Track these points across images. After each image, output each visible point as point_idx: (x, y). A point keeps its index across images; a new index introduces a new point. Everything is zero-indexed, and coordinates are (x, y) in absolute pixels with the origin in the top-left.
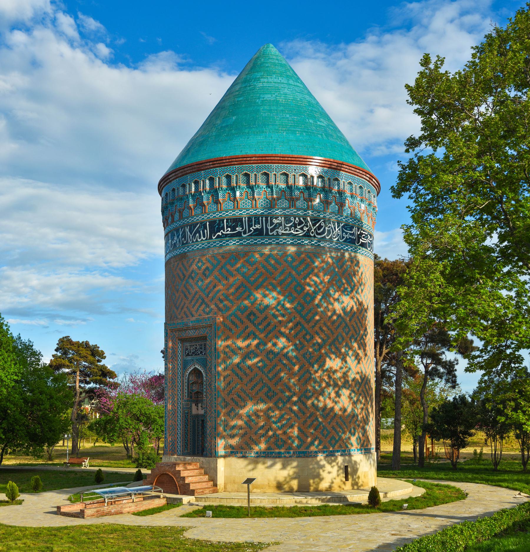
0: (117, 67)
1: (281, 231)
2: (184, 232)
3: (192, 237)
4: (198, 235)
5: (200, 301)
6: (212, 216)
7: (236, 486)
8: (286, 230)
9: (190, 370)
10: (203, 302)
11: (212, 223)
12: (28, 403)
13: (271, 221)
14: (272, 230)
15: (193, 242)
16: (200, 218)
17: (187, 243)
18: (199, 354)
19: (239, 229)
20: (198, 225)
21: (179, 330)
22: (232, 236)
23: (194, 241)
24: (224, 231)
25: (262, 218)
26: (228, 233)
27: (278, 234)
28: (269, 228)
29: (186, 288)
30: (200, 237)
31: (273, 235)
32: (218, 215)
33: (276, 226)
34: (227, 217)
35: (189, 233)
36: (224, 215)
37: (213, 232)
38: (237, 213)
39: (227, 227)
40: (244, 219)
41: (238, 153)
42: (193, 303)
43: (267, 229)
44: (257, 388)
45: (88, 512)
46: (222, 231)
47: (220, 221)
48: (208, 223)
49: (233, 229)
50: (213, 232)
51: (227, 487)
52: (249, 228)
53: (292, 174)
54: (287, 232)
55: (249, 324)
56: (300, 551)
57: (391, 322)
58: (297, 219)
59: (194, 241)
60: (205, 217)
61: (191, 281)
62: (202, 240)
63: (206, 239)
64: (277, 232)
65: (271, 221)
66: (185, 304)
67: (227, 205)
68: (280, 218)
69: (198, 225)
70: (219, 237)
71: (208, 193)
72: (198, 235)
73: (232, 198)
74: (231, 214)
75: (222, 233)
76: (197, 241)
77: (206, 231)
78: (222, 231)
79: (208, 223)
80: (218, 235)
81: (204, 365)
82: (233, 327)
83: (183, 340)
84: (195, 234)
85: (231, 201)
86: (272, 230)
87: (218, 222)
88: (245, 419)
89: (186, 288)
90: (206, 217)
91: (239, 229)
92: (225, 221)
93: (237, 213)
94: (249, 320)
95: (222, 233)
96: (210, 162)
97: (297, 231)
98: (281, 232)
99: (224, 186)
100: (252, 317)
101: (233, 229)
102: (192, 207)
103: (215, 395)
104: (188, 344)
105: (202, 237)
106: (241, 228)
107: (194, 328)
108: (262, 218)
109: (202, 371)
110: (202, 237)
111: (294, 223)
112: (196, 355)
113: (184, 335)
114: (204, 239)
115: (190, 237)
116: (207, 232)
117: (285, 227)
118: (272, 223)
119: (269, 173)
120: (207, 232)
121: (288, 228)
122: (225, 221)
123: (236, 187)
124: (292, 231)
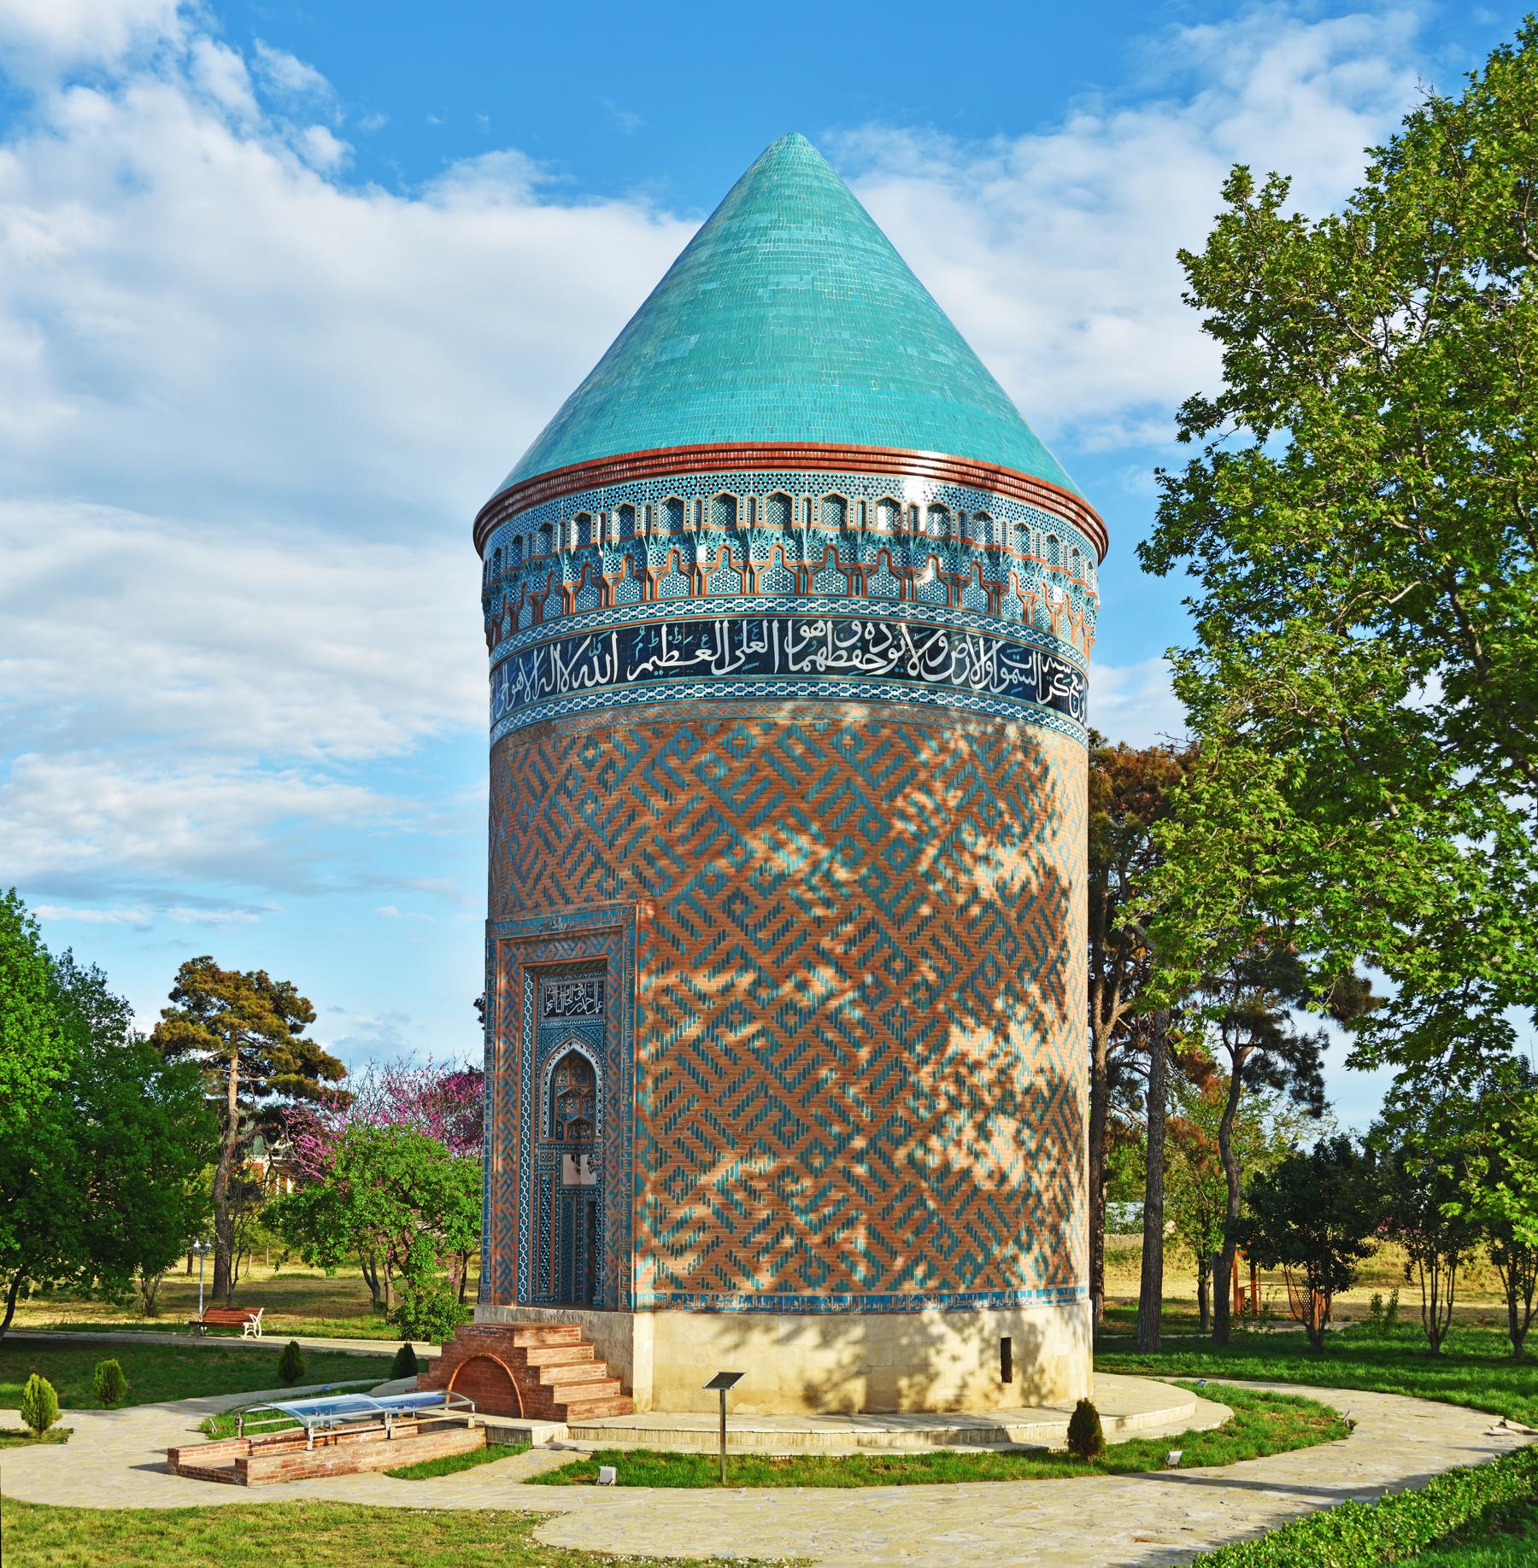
0: (362, 194)
1: (822, 660)
2: (547, 659)
4: (585, 668)
5: (590, 858)
6: (626, 617)
7: (687, 1394)
8: (839, 658)
9: (558, 1057)
10: (598, 861)
11: (627, 635)
13: (796, 631)
14: (798, 658)
15: (571, 688)
16: (592, 622)
17: (553, 691)
18: (583, 1012)
19: (703, 654)
20: (588, 642)
21: (528, 942)
22: (682, 671)
23: (576, 685)
25: (770, 622)
26: (672, 663)
27: (814, 670)
28: (791, 651)
29: (551, 822)
30: (591, 676)
31: (801, 671)
32: (643, 615)
33: (809, 645)
34: (671, 619)
35: (559, 663)
36: (661, 613)
37: (627, 662)
38: (699, 607)
39: (670, 647)
40: (717, 625)
41: (703, 438)
42: (568, 865)
43: (783, 654)
44: (751, 1111)
45: (256, 1467)
46: (655, 658)
47: (648, 629)
48: (614, 636)
49: (688, 653)
50: (627, 662)
51: (662, 1398)
52: (732, 651)
53: (644, 503)
54: (842, 664)
55: (730, 926)
58: (870, 626)
59: (576, 685)
60: (607, 619)
61: (563, 801)
62: (598, 684)
63: (610, 682)
64: (813, 663)
65: (796, 631)
66: (545, 865)
67: (670, 585)
68: (820, 624)
69: (588, 642)
70: (645, 675)
71: (617, 550)
72: (585, 668)
73: (685, 565)
74: (680, 612)
75: (654, 663)
76: (582, 686)
77: (608, 658)
78: (655, 658)
79: (614, 636)
80: (645, 670)
81: (600, 1046)
82: (684, 935)
83: (537, 972)
85: (681, 573)
86: (798, 658)
87: (643, 633)
89: (551, 822)
90: (609, 617)
91: (703, 654)
92: (664, 629)
93: (699, 610)
94: (730, 914)
95: (654, 663)
96: (622, 462)
97: (869, 661)
98: (824, 663)
99: (664, 532)
100: (738, 907)
101: (688, 653)
102: (571, 590)
103: (630, 1130)
104: (552, 983)
105: (598, 676)
107: (571, 937)
108: (770, 622)
109: (593, 1061)
110: (598, 676)
111: (862, 638)
112: (575, 1013)
113: (541, 956)
115: (562, 675)
116: (612, 662)
117: (836, 648)
118: (798, 639)
119: (589, 512)
120: (612, 662)
121: (844, 654)
122: (664, 629)
123: (698, 533)
124: (856, 662)
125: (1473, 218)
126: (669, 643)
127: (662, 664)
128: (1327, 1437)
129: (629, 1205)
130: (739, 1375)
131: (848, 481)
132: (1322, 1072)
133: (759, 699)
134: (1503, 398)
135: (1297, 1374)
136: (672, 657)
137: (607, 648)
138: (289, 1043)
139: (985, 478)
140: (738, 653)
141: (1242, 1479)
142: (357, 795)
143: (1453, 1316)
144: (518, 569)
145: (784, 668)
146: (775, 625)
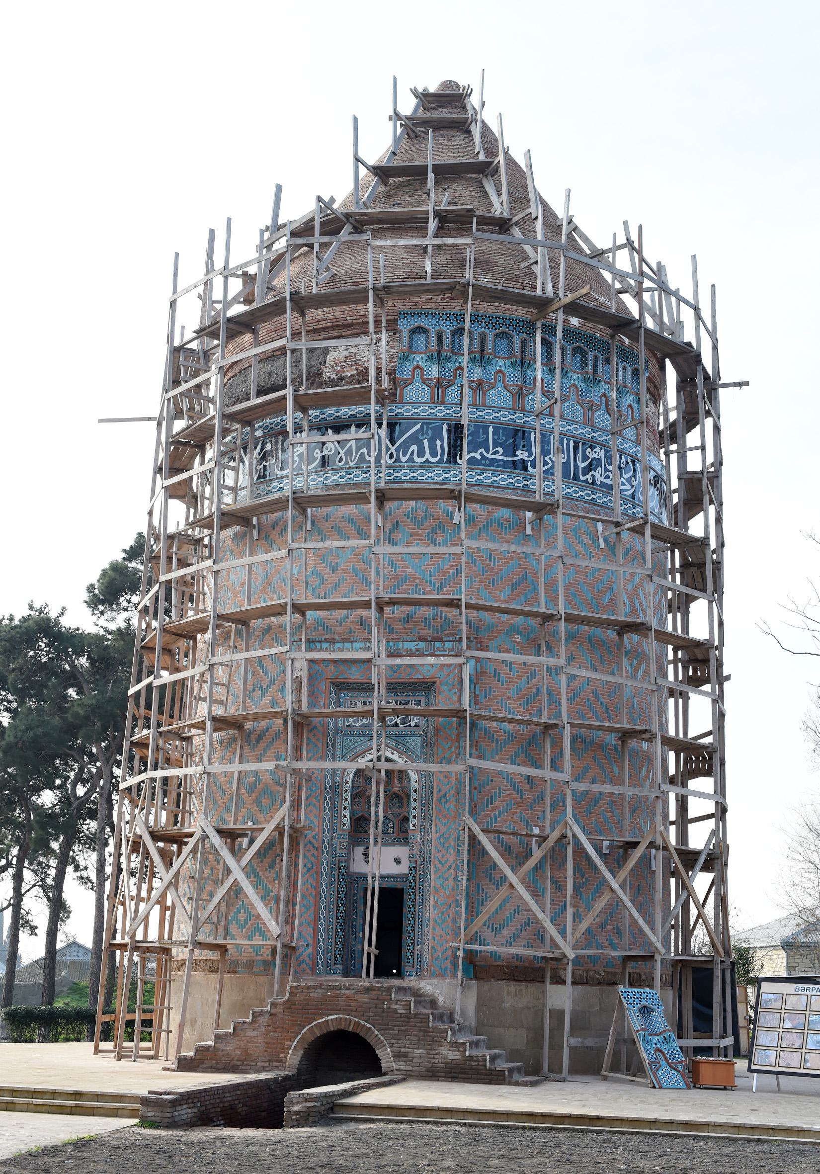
3: (397, 450)
4: (414, 447)
8: (607, 477)
12: (60, 787)
13: (584, 452)
19: (521, 454)
20: (418, 427)
22: (505, 464)
24: (488, 452)
25: (568, 440)
26: (497, 457)
27: (593, 483)
30: (421, 454)
31: (586, 481)
36: (489, 415)
38: (440, 411)
39: (496, 444)
43: (576, 466)
46: (482, 450)
56: (105, 1172)
57: (106, 836)
59: (404, 459)
62: (427, 461)
63: (441, 461)
65: (584, 452)
68: (597, 449)
69: (418, 427)
72: (414, 447)
75: (481, 454)
77: (439, 443)
78: (482, 450)
84: (406, 446)
87: (161, 844)
88: (493, 1068)
91: (521, 454)
92: (491, 430)
95: (481, 454)
98: (600, 478)
105: (428, 455)
106: (526, 454)
108: (568, 440)
110: (428, 455)
114: (432, 460)
118: (585, 458)
122: (491, 430)
125: (511, 328)
126: (494, 439)
127: (489, 456)
128: (544, 841)
129: (599, 506)
130: (278, 185)
131: (644, 996)
132: (86, 632)
133: (317, 880)
134: (152, 543)
135: (321, 337)
136: (497, 452)
137: (438, 434)
138: (462, 545)
139: (168, 1032)
140: (547, 459)
141: (774, 975)
142: (714, 888)
143: (62, 973)
144: (28, 678)
145: (576, 477)
146: (572, 444)
